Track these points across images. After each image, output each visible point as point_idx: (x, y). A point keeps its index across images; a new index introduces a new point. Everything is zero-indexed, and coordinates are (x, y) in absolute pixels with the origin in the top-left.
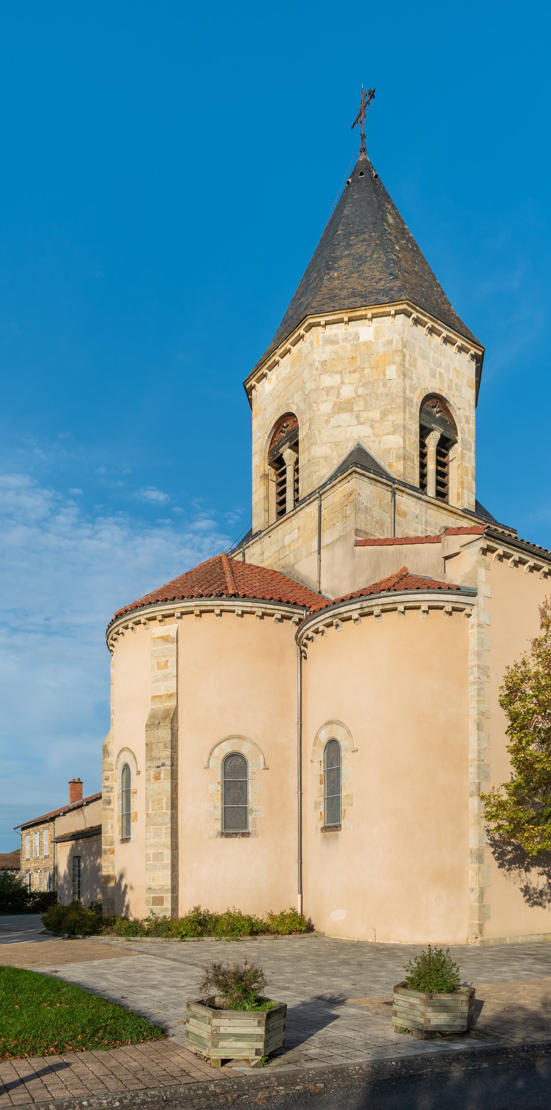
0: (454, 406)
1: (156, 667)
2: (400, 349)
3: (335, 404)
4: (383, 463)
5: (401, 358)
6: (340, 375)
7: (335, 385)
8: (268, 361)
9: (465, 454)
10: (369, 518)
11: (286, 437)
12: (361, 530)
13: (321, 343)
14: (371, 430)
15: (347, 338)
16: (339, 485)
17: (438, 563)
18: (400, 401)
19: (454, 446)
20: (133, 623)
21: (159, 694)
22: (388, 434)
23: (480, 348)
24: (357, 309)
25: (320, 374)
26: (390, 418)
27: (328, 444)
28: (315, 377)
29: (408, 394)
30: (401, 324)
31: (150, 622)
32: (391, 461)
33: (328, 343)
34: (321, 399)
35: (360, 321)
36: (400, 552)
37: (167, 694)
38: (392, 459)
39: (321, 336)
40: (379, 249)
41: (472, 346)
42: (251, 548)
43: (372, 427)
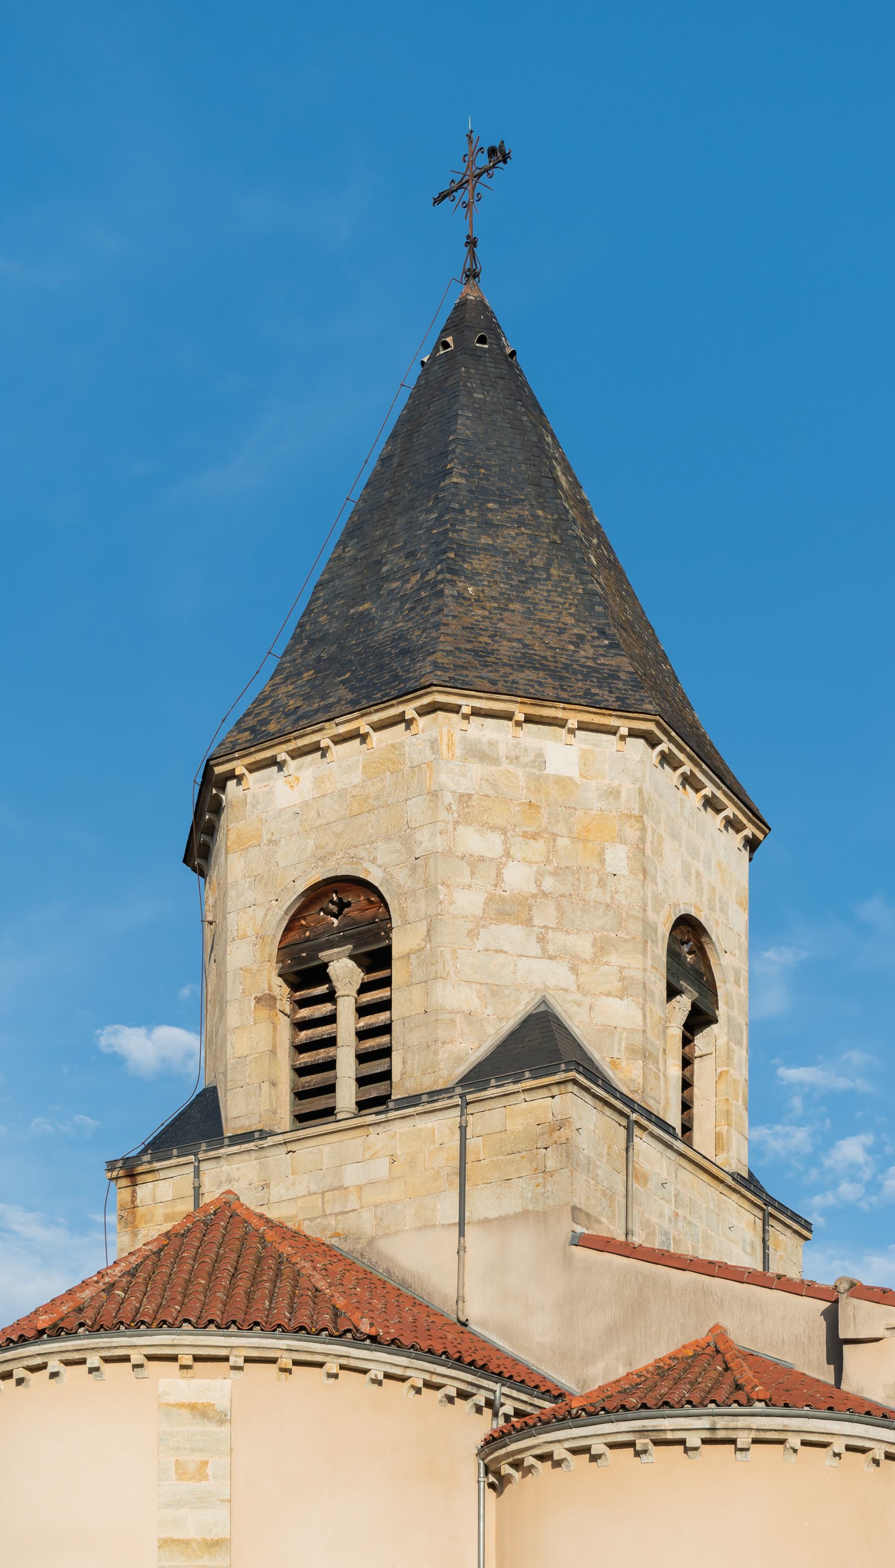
0: (716, 944)
1: (173, 1472)
2: (636, 812)
3: (490, 899)
4: (600, 1056)
5: (638, 833)
6: (503, 837)
7: (490, 855)
8: (295, 738)
9: (733, 1051)
10: (593, 1182)
11: (339, 929)
12: (581, 1210)
13: (458, 752)
14: (572, 977)
15: (517, 757)
16: (522, 1096)
17: (809, 1338)
18: (636, 928)
19: (709, 1029)
20: (101, 1357)
21: (182, 1537)
22: (609, 994)
23: (763, 826)
24: (547, 703)
25: (457, 823)
26: (614, 959)
27: (474, 986)
28: (443, 824)
29: (651, 916)
30: (638, 759)
31: (151, 1363)
32: (616, 1055)
33: (475, 756)
34: (459, 880)
35: (547, 727)
36: (707, 1292)
37: (205, 1541)
38: (618, 1050)
39: (457, 736)
40: (562, 557)
41: (750, 820)
42: (223, 1161)
43: (574, 970)
